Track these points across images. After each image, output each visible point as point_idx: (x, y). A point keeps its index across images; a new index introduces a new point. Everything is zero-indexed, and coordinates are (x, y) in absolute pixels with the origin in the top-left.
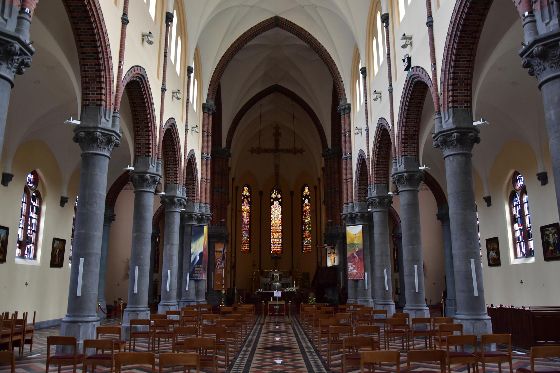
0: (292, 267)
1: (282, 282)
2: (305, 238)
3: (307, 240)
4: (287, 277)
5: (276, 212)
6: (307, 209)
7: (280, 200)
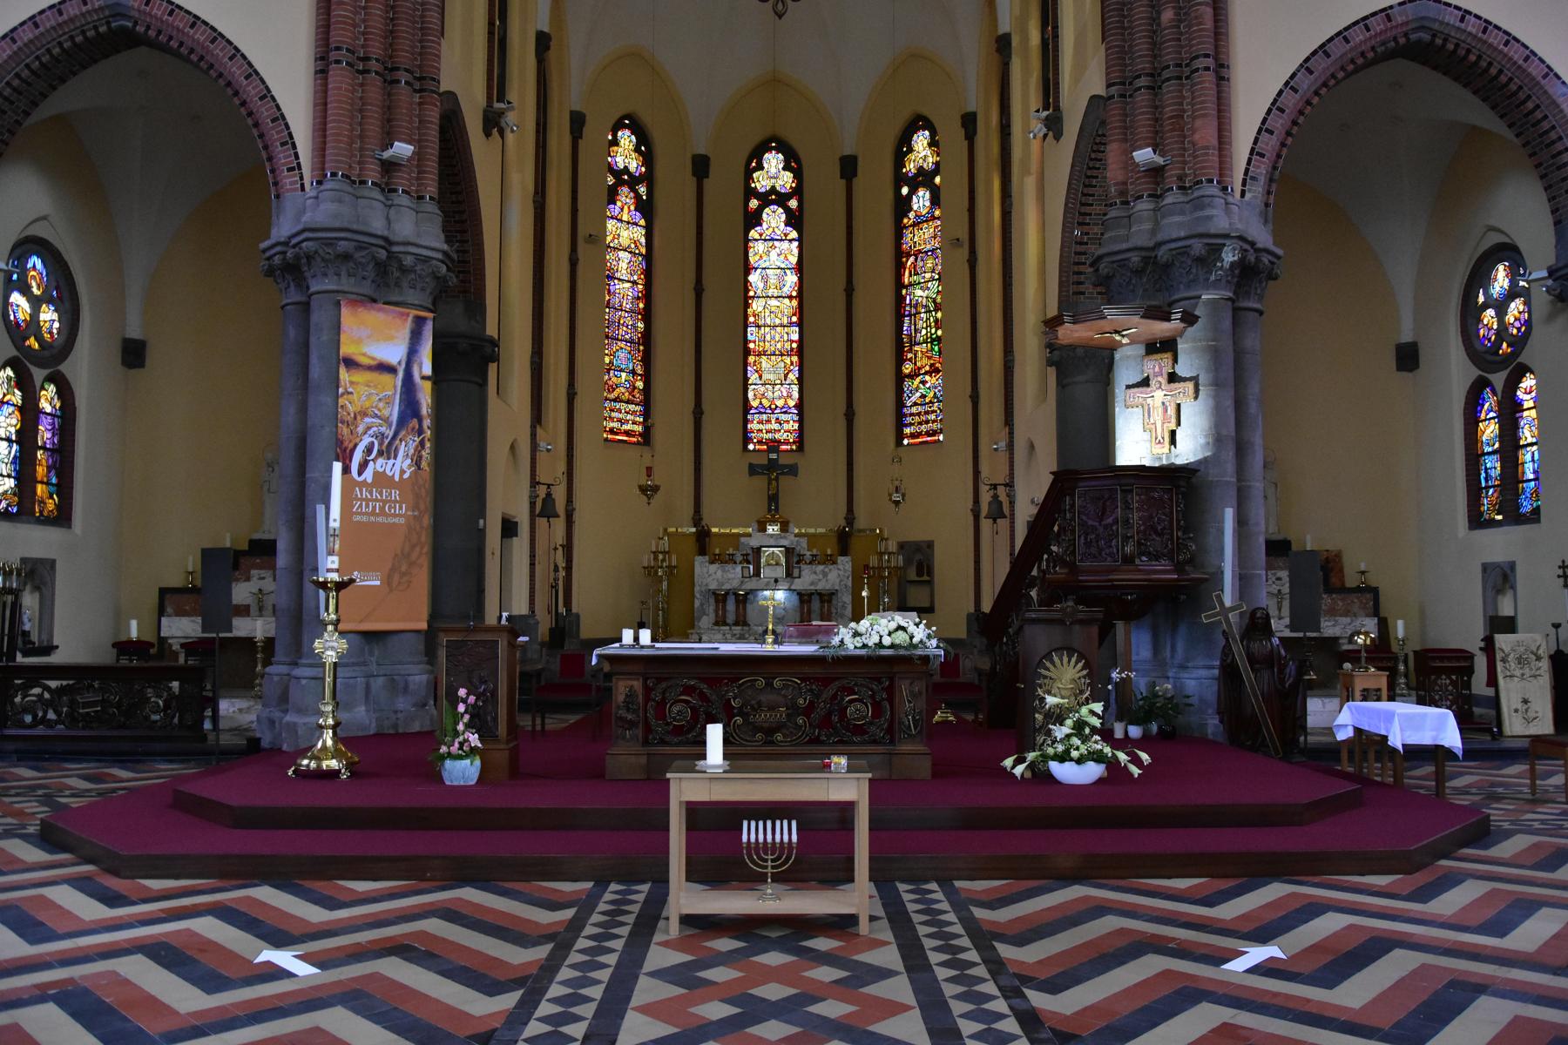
0: (850, 518)
1: (801, 584)
2: (912, 376)
3: (923, 389)
4: (830, 560)
5: (774, 255)
6: (922, 237)
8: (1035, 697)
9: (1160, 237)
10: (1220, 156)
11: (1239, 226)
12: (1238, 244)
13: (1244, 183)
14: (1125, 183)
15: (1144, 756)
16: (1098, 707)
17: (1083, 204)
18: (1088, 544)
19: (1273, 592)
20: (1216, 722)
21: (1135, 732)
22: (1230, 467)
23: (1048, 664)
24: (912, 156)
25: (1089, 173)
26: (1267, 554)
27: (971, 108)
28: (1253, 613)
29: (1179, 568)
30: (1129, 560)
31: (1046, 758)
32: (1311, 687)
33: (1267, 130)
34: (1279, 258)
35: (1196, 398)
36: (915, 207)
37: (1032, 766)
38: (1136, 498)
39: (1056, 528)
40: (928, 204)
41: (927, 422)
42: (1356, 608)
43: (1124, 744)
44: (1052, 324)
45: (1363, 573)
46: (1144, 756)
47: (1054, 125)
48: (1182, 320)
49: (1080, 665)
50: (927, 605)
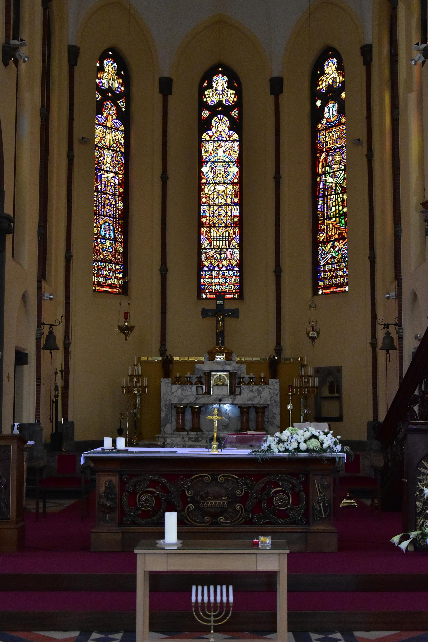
0: (279, 349)
1: (239, 400)
2: (325, 242)
4: (263, 382)
5: (221, 151)
7: (235, 113)
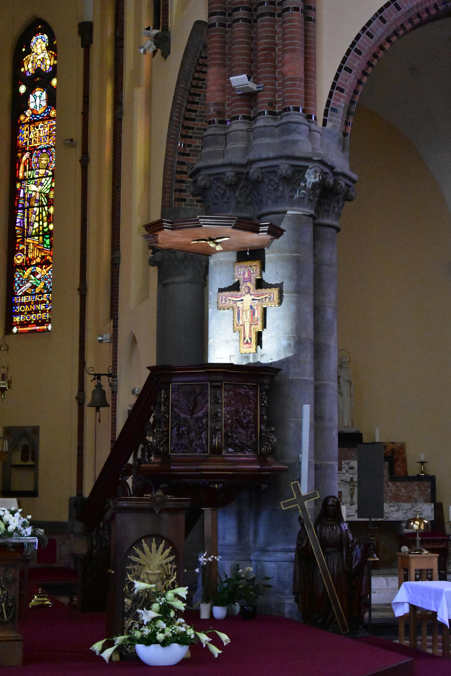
2: (24, 267)
3: (34, 280)
6: (37, 135)
8: (123, 581)
9: (251, 157)
10: (306, 87)
11: (321, 151)
12: (319, 167)
13: (326, 114)
14: (223, 104)
15: (224, 637)
16: (183, 591)
17: (186, 119)
18: (180, 436)
19: (343, 481)
20: (292, 601)
21: (220, 612)
22: (309, 368)
23: (138, 551)
24: (31, 57)
25: (192, 91)
26: (340, 446)
27: (89, 18)
28: (326, 501)
29: (262, 459)
30: (216, 451)
31: (133, 641)
32: (376, 566)
33: (346, 69)
34: (354, 181)
35: (280, 303)
36: (32, 106)
37: (120, 649)
38: (224, 394)
39: (151, 420)
40: (44, 104)
41: (36, 312)
42: (416, 494)
43: (210, 625)
44: (153, 228)
45: (422, 463)
46: (224, 637)
47: (162, 43)
48: (269, 232)
49: (168, 551)
50: (31, 489)
